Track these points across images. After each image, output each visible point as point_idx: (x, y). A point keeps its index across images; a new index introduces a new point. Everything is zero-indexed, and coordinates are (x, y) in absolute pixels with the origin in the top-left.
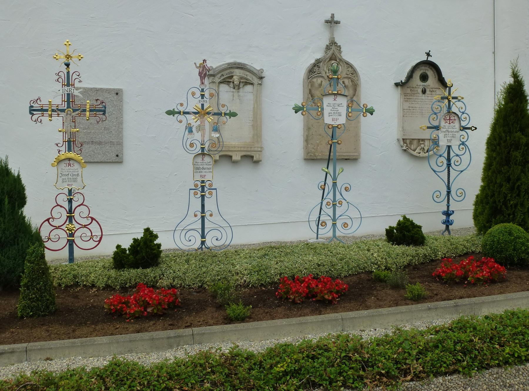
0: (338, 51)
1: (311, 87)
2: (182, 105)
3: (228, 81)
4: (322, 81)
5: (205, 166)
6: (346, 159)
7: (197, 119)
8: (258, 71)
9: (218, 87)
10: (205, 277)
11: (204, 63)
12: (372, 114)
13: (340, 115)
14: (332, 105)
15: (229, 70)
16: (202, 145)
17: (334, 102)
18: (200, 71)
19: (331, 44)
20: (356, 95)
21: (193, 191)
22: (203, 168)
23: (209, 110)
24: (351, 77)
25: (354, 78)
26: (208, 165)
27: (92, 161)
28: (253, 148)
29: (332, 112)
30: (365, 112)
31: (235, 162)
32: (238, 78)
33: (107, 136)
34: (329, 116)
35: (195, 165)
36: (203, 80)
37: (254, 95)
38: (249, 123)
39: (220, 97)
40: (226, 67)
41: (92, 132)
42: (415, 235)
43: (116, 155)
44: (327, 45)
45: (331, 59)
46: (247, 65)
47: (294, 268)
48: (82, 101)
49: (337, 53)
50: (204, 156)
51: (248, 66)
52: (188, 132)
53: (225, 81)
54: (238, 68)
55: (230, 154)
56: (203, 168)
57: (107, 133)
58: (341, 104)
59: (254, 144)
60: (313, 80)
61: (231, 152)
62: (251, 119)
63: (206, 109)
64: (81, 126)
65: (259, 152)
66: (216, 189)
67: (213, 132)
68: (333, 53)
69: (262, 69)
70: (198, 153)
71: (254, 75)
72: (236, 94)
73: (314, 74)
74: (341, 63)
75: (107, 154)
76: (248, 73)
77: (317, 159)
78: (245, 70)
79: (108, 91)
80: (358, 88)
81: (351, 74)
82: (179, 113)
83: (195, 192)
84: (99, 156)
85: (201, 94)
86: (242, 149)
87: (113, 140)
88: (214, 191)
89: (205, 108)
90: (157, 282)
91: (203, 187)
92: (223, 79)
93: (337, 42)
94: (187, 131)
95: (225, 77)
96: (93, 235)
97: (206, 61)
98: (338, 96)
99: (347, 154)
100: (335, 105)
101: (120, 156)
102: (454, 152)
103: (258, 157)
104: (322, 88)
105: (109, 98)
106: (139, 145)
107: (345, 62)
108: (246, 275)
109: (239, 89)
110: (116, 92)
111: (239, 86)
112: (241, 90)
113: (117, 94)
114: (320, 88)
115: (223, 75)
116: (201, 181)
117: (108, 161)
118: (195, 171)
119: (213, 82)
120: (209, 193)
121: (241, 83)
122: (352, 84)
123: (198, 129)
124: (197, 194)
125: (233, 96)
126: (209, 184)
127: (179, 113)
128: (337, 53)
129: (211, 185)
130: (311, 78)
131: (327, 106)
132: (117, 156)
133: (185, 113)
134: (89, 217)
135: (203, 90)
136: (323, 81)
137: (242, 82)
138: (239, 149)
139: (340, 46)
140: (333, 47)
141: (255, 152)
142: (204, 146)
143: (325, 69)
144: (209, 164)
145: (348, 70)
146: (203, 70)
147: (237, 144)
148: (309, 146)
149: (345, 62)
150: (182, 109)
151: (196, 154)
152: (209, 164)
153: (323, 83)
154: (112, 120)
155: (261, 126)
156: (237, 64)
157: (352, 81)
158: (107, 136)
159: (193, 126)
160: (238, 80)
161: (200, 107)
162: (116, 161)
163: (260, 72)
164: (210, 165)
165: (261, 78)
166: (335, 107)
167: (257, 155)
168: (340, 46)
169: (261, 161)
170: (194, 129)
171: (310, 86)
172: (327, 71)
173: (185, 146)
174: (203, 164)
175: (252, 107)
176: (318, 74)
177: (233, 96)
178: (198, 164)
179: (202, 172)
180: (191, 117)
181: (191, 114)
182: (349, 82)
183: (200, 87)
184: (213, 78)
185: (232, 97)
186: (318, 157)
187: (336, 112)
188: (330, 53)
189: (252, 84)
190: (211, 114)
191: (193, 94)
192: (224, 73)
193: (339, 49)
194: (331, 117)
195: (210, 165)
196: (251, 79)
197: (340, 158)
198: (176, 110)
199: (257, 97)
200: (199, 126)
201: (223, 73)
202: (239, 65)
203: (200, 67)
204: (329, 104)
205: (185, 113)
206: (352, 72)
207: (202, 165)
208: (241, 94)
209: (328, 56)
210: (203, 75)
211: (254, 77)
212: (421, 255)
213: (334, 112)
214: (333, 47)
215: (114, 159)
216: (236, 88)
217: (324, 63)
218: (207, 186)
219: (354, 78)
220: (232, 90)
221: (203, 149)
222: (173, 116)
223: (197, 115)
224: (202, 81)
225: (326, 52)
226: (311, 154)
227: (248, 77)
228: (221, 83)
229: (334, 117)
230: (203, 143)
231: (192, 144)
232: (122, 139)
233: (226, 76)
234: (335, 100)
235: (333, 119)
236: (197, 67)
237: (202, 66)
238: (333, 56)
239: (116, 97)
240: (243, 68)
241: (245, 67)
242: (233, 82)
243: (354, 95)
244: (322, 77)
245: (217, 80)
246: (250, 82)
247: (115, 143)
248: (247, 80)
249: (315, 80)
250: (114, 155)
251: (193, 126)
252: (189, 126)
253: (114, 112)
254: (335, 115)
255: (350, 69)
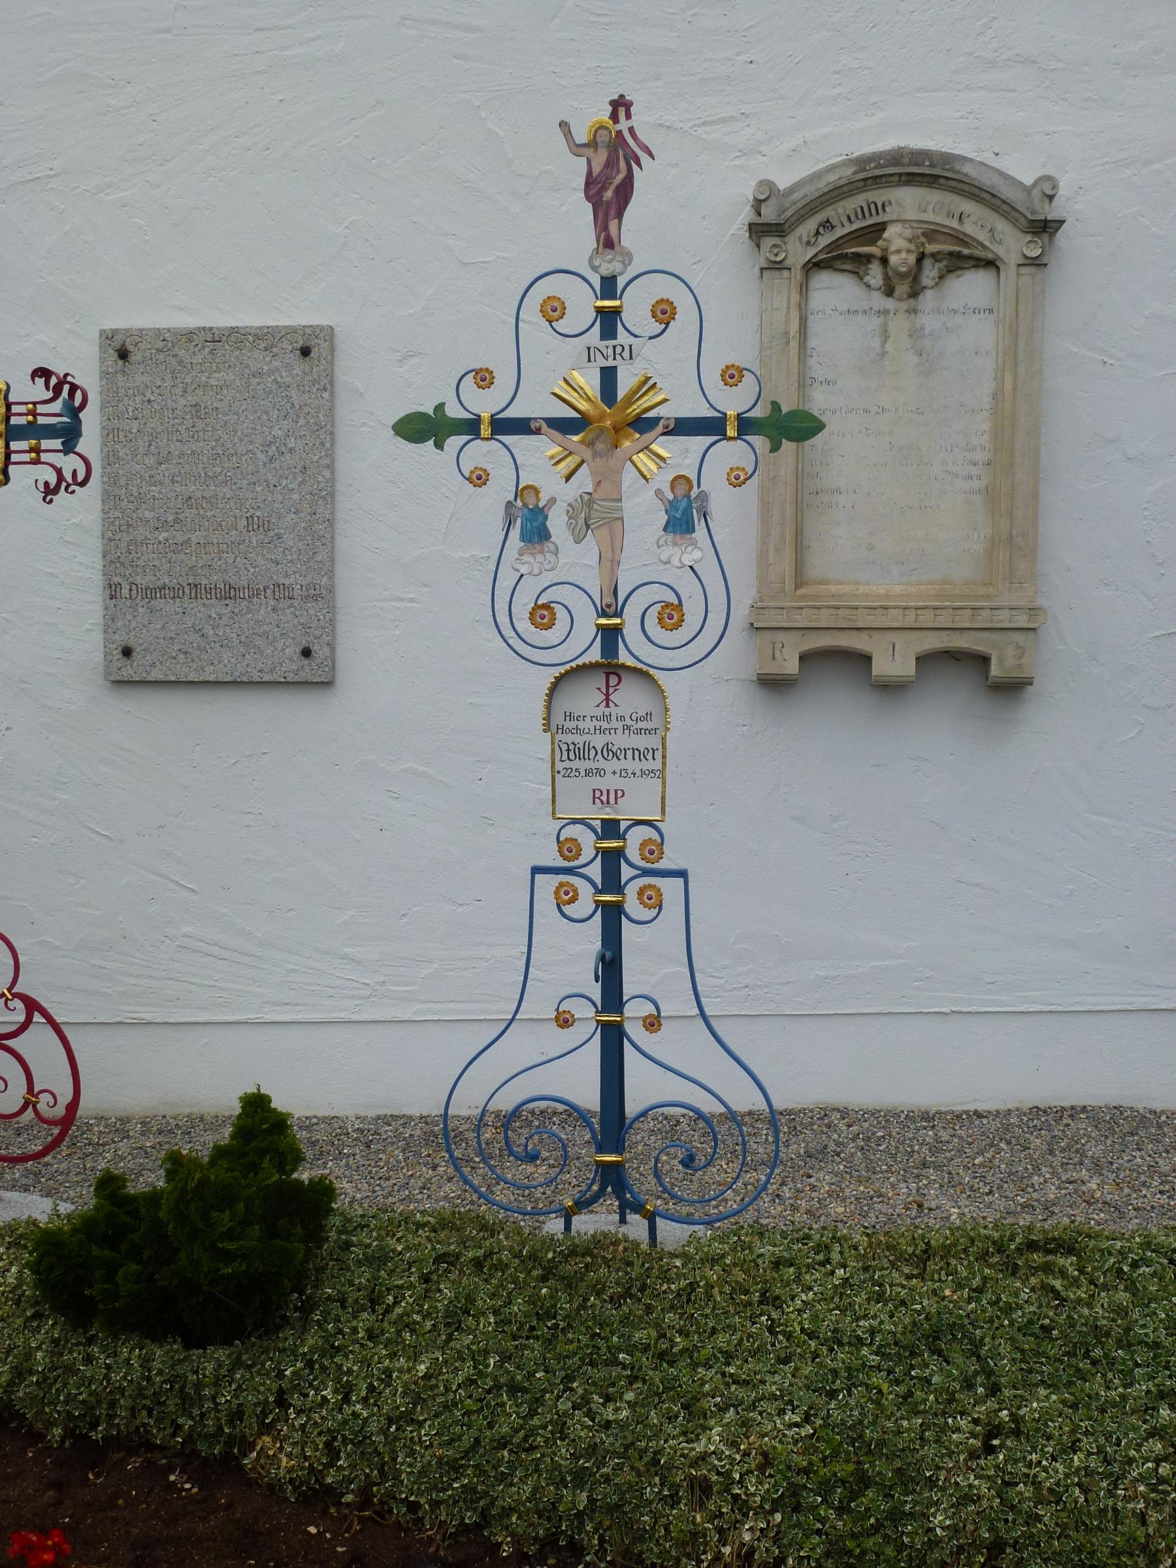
2: (484, 378)
5: (621, 740)
7: (571, 462)
8: (1028, 190)
9: (804, 289)
10: (502, 1478)
11: (614, 117)
15: (864, 195)
16: (604, 614)
18: (597, 170)
21: (547, 884)
22: (609, 752)
23: (644, 403)
26: (639, 731)
27: (193, 677)
31: (890, 688)
32: (908, 233)
33: (260, 561)
35: (561, 729)
36: (613, 225)
37: (997, 323)
38: (970, 477)
39: (812, 343)
40: (843, 182)
41: (194, 540)
43: (298, 650)
46: (965, 159)
47: (1104, 1511)
48: (148, 395)
50: (613, 680)
51: (967, 169)
52: (523, 538)
53: (844, 257)
54: (910, 179)
55: (859, 643)
56: (609, 752)
57: (261, 544)
59: (991, 590)
61: (864, 635)
62: (981, 456)
63: (630, 399)
64: (148, 514)
65: (1018, 637)
66: (682, 874)
67: (670, 537)
69: (1048, 178)
70: (574, 664)
71: (1005, 216)
72: (899, 325)
75: (259, 642)
76: (967, 206)
79: (266, 338)
82: (471, 427)
83: (561, 885)
84: (226, 655)
85: (600, 311)
86: (926, 619)
87: (286, 575)
88: (671, 888)
89: (621, 393)
90: (247, 1446)
91: (612, 860)
92: (831, 247)
94: (515, 533)
95: (839, 232)
96: (36, 1090)
97: (628, 105)
101: (320, 652)
102: (585, 328)
103: (1010, 661)
105: (271, 372)
106: (412, 600)
108: (760, 1511)
109: (914, 294)
110: (301, 343)
111: (914, 276)
112: (928, 299)
113: (305, 352)
115: (827, 225)
116: (597, 824)
117: (267, 678)
118: (559, 766)
119: (776, 266)
120: (641, 893)
121: (927, 263)
123: (581, 521)
124: (573, 900)
125: (885, 335)
126: (643, 844)
127: (471, 427)
129: (653, 849)
132: (307, 653)
133: (503, 426)
134: (15, 996)
135: (609, 287)
137: (933, 255)
138: (910, 620)
141: (996, 636)
142: (618, 621)
144: (641, 725)
146: (611, 163)
147: (898, 589)
150: (484, 404)
151: (567, 667)
152: (641, 725)
154: (284, 482)
155: (1035, 496)
156: (906, 160)
158: (260, 561)
159: (553, 501)
161: (590, 382)
162: (302, 676)
164: (648, 731)
165: (1045, 228)
167: (1010, 651)
169: (1028, 682)
170: (557, 523)
173: (503, 619)
174: (605, 725)
175: (988, 387)
177: (885, 335)
178: (581, 725)
179: (600, 772)
180: (546, 446)
181: (538, 431)
183: (595, 269)
184: (777, 241)
185: (876, 343)
189: (991, 264)
190: (660, 429)
191: (553, 311)
195: (648, 731)
196: (982, 236)
198: (454, 411)
199: (1015, 336)
200: (588, 501)
201: (828, 213)
202: (917, 164)
203: (593, 144)
205: (503, 426)
207: (602, 731)
210: (609, 194)
211: (1002, 225)
215: (292, 666)
216: (902, 289)
218: (633, 853)
220: (879, 301)
221: (610, 636)
222: (439, 446)
223: (576, 438)
224: (605, 228)
227: (969, 228)
228: (814, 266)
230: (609, 599)
231: (546, 606)
232: (331, 575)
233: (849, 228)
236: (576, 149)
237: (603, 137)
239: (299, 366)
241: (952, 170)
242: (884, 261)
245: (797, 251)
246: (978, 253)
247: (297, 592)
248: (965, 243)
250: (293, 651)
251: (553, 501)
252: (525, 505)
253: (291, 443)
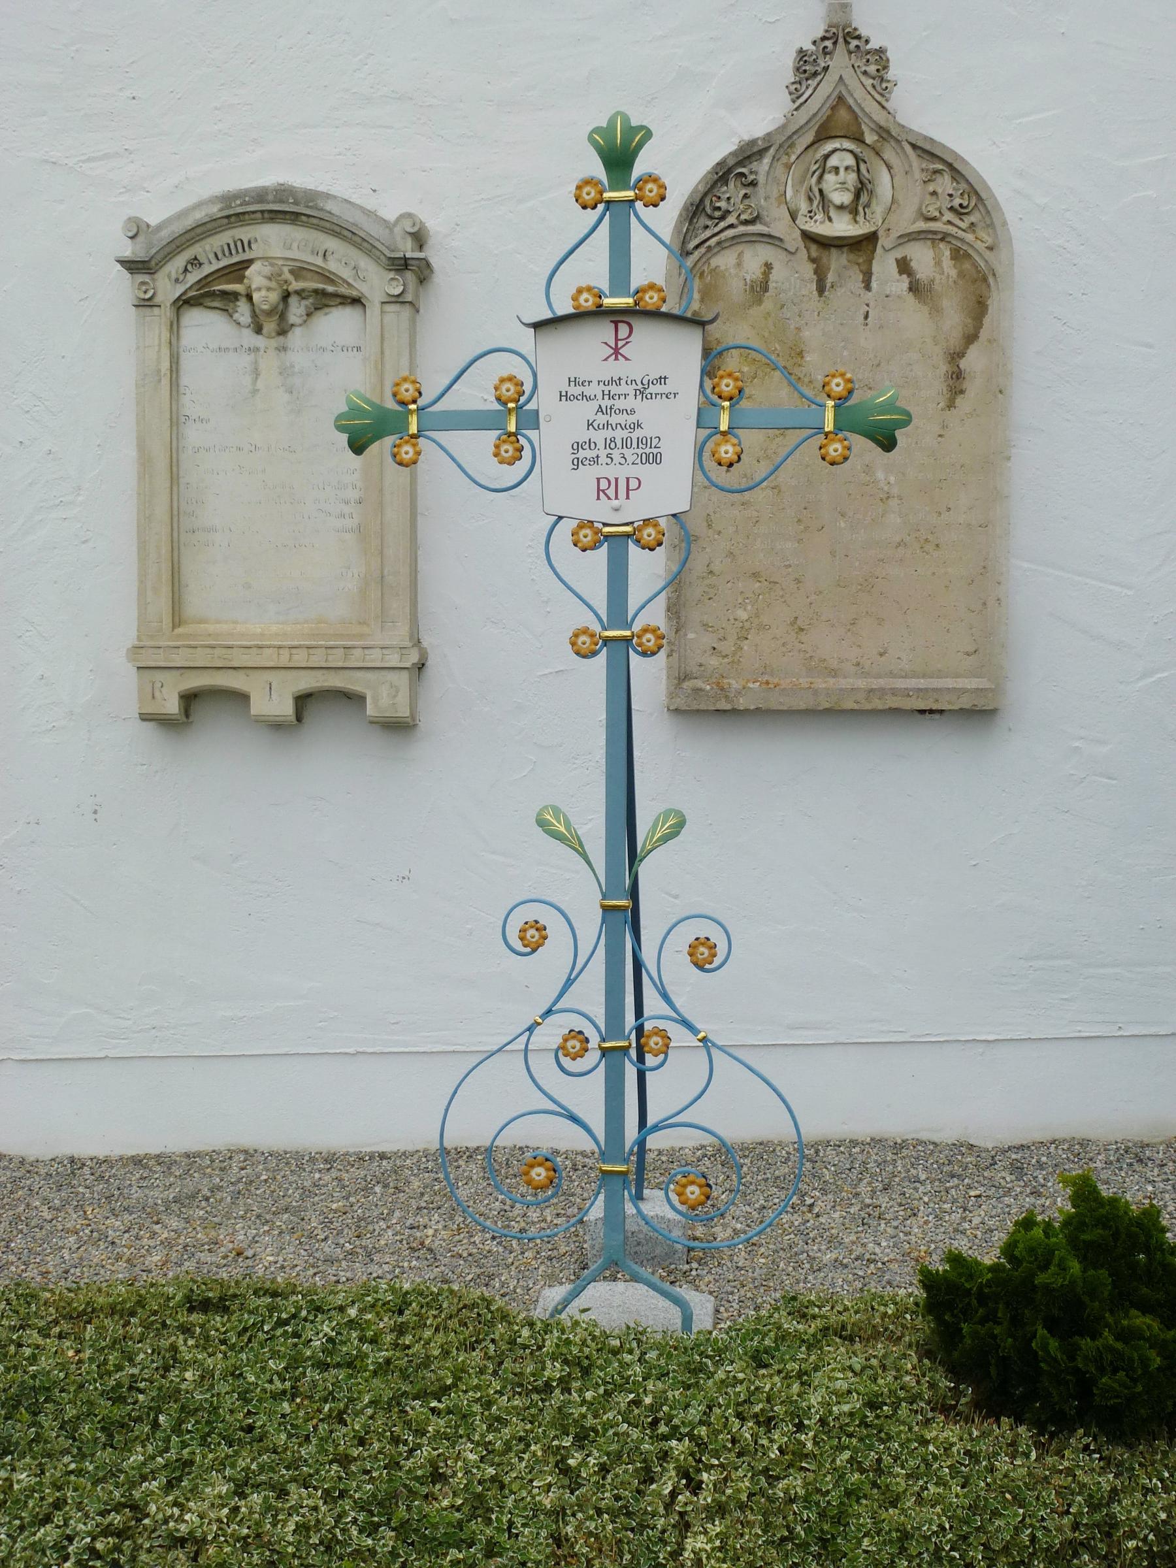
0: (869, 82)
1: (702, 300)
3: (224, 293)
4: (768, 267)
6: (922, 712)
9: (175, 327)
12: (888, 444)
13: (655, 459)
14: (594, 390)
17: (616, 368)
19: (828, 43)
20: (984, 334)
24: (952, 230)
25: (969, 237)
28: (357, 653)
29: (599, 437)
30: (838, 428)
34: (577, 464)
42: (1102, 1370)
44: (802, 54)
45: (824, 134)
46: (328, 196)
49: (860, 95)
51: (329, 206)
53: (212, 295)
54: (274, 216)
58: (663, 380)
59: (366, 630)
60: (714, 262)
61: (241, 674)
68: (841, 98)
72: (270, 362)
73: (722, 225)
74: (889, 154)
76: (331, 243)
77: (735, 712)
78: (317, 228)
80: (994, 294)
81: (948, 216)
86: (300, 658)
93: (864, 32)
95: (207, 269)
98: (636, 324)
99: (922, 683)
100: (614, 389)
104: (768, 304)
107: (914, 146)
109: (283, 332)
111: (280, 313)
112: (296, 337)
114: (759, 302)
115: (195, 262)
121: (293, 300)
122: (961, 274)
125: (256, 373)
128: (859, 93)
130: (702, 250)
131: (564, 396)
136: (777, 266)
137: (298, 293)
138: (284, 660)
139: (881, 52)
140: (840, 62)
141: (370, 675)
143: (789, 194)
145: (934, 193)
147: (274, 628)
148: (691, 636)
149: (914, 146)
153: (774, 276)
156: (270, 197)
157: (958, 255)
160: (265, 282)
163: (397, 230)
166: (620, 404)
167: (384, 691)
168: (881, 52)
171: (696, 296)
172: (804, 207)
176: (746, 222)
177: (256, 373)
182: (938, 263)
184: (146, 278)
185: (247, 380)
186: (742, 703)
187: (625, 434)
188: (821, 94)
189: (356, 301)
192: (204, 249)
193: (872, 69)
194: (589, 474)
196: (346, 273)
197: (878, 704)
202: (282, 201)
204: (576, 382)
206: (957, 202)
208: (298, 358)
209: (802, 117)
212: (1131, 1544)
213: (609, 433)
214: (840, 62)
217: (784, 159)
219: (969, 237)
220: (249, 338)
225: (795, 95)
226: (699, 683)
227: (333, 266)
228: (184, 303)
229: (611, 472)
233: (216, 265)
234: (617, 352)
235: (604, 485)
238: (843, 113)
240: (297, 215)
242: (249, 297)
243: (971, 338)
244: (769, 239)
246: (343, 290)
248: (332, 282)
249: (724, 261)
254: (617, 457)
255: (945, 184)
